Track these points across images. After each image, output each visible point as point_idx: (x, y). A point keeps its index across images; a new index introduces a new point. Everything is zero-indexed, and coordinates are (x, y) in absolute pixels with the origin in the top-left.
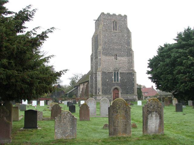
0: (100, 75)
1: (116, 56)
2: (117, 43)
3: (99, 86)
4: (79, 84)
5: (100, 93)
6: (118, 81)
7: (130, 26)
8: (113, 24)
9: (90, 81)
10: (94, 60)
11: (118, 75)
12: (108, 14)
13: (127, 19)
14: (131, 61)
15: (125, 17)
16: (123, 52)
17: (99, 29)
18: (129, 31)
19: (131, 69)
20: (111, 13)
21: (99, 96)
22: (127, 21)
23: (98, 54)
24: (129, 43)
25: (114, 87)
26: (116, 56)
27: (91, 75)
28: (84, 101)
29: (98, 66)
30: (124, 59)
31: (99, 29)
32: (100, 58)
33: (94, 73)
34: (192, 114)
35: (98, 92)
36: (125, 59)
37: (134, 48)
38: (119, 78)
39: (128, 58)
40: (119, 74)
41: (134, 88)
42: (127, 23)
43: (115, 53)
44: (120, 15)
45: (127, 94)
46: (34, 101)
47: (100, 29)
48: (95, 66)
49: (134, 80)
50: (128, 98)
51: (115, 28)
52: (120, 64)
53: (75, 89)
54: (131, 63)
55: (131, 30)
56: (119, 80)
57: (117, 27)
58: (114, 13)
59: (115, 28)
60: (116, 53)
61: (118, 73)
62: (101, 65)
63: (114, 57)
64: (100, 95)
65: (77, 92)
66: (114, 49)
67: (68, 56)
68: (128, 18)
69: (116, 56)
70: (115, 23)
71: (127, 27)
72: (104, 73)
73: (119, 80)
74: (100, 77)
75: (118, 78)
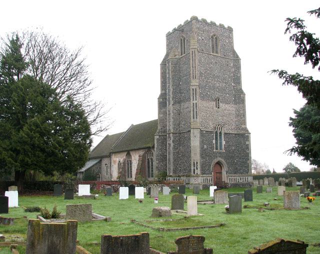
0: (198, 135)
1: (218, 101)
2: (218, 77)
3: (196, 156)
4: (110, 153)
5: (198, 171)
6: (221, 149)
7: (237, 48)
8: (212, 41)
9: (156, 146)
10: (170, 107)
11: (221, 138)
12: (204, 21)
13: (232, 35)
14: (242, 112)
15: (230, 30)
16: (228, 95)
17: (191, 47)
18: (238, 57)
19: (243, 126)
20: (209, 21)
21: (195, 178)
22: (232, 38)
23: (192, 94)
24: (237, 80)
25: (216, 161)
26: (217, 102)
27: (158, 137)
28: (253, 192)
29: (192, 118)
30: (228, 108)
31: (191, 47)
32: (195, 102)
33: (172, 131)
34: (318, 207)
35: (192, 168)
36: (231, 109)
37: (245, 86)
38: (224, 143)
39: (236, 106)
40: (223, 136)
41: (248, 162)
42: (233, 43)
43: (217, 96)
44: (221, 26)
45: (235, 173)
46: (6, 194)
47: (194, 47)
48: (173, 118)
49: (248, 148)
50: (237, 181)
51: (215, 48)
52: (225, 118)
53: (96, 163)
54: (241, 116)
55: (240, 56)
56: (223, 147)
57: (219, 47)
58: (214, 20)
59: (215, 48)
60: (218, 95)
61: (220, 133)
62: (198, 116)
63: (215, 103)
64: (197, 176)
65: (100, 168)
66: (214, 88)
67: (119, 97)
68: (234, 33)
69: (218, 101)
70: (215, 39)
71: (233, 47)
72: (202, 134)
73: (223, 147)
74: (198, 139)
75: (221, 143)
